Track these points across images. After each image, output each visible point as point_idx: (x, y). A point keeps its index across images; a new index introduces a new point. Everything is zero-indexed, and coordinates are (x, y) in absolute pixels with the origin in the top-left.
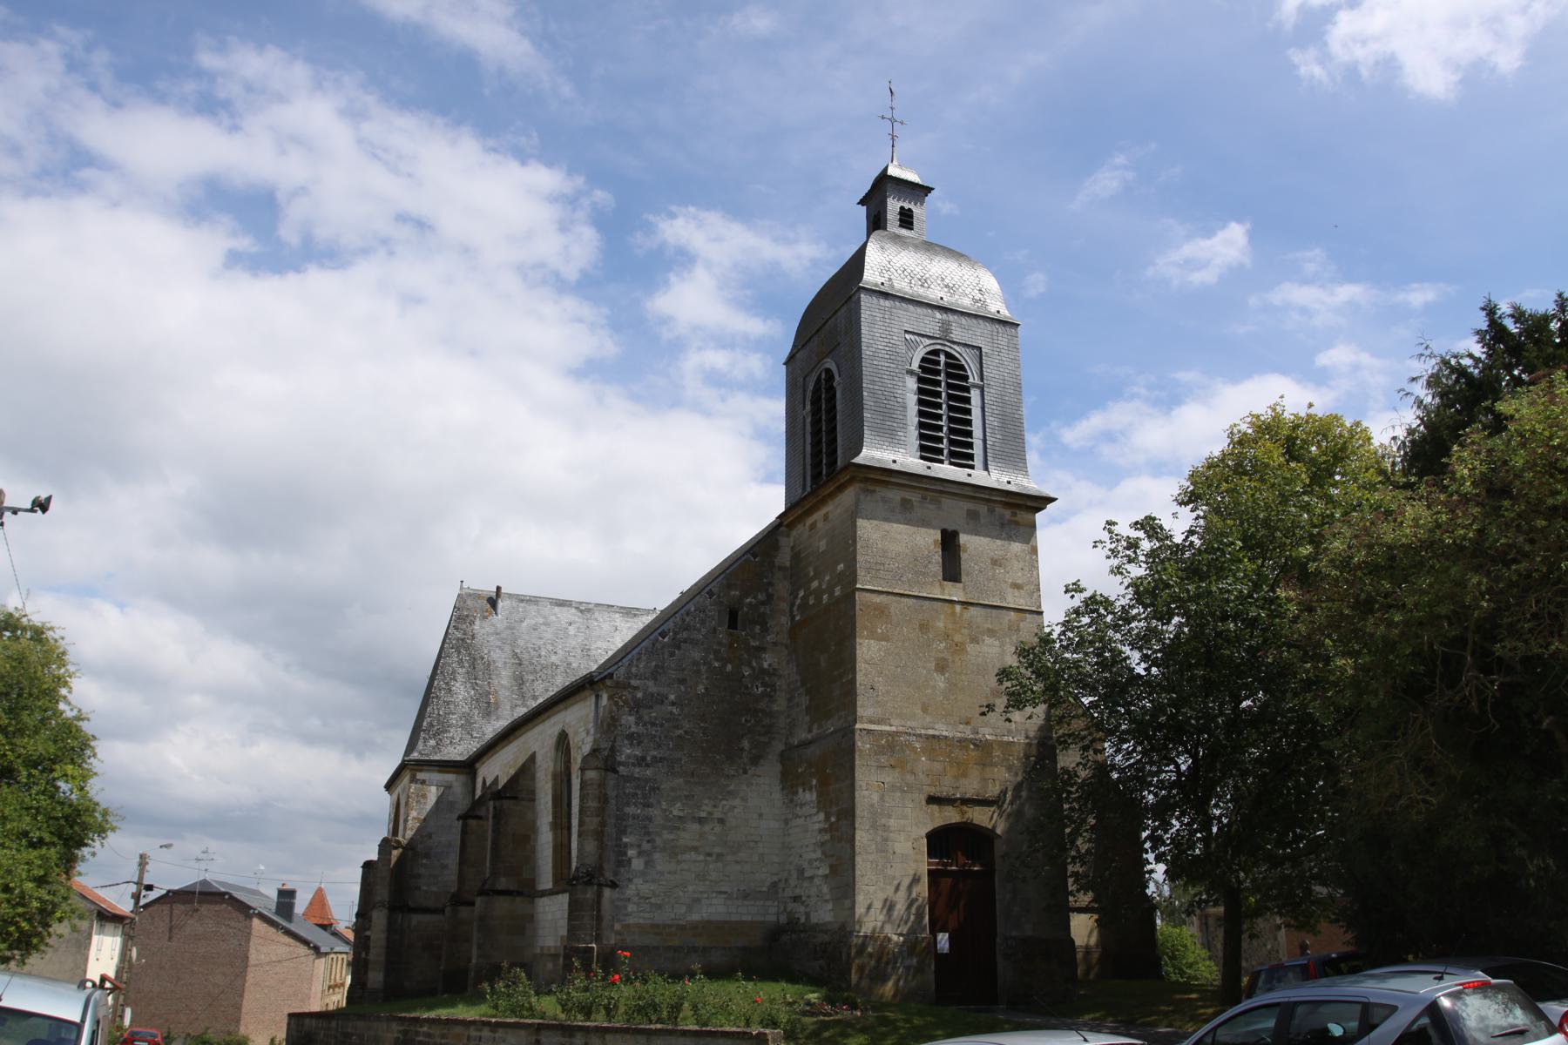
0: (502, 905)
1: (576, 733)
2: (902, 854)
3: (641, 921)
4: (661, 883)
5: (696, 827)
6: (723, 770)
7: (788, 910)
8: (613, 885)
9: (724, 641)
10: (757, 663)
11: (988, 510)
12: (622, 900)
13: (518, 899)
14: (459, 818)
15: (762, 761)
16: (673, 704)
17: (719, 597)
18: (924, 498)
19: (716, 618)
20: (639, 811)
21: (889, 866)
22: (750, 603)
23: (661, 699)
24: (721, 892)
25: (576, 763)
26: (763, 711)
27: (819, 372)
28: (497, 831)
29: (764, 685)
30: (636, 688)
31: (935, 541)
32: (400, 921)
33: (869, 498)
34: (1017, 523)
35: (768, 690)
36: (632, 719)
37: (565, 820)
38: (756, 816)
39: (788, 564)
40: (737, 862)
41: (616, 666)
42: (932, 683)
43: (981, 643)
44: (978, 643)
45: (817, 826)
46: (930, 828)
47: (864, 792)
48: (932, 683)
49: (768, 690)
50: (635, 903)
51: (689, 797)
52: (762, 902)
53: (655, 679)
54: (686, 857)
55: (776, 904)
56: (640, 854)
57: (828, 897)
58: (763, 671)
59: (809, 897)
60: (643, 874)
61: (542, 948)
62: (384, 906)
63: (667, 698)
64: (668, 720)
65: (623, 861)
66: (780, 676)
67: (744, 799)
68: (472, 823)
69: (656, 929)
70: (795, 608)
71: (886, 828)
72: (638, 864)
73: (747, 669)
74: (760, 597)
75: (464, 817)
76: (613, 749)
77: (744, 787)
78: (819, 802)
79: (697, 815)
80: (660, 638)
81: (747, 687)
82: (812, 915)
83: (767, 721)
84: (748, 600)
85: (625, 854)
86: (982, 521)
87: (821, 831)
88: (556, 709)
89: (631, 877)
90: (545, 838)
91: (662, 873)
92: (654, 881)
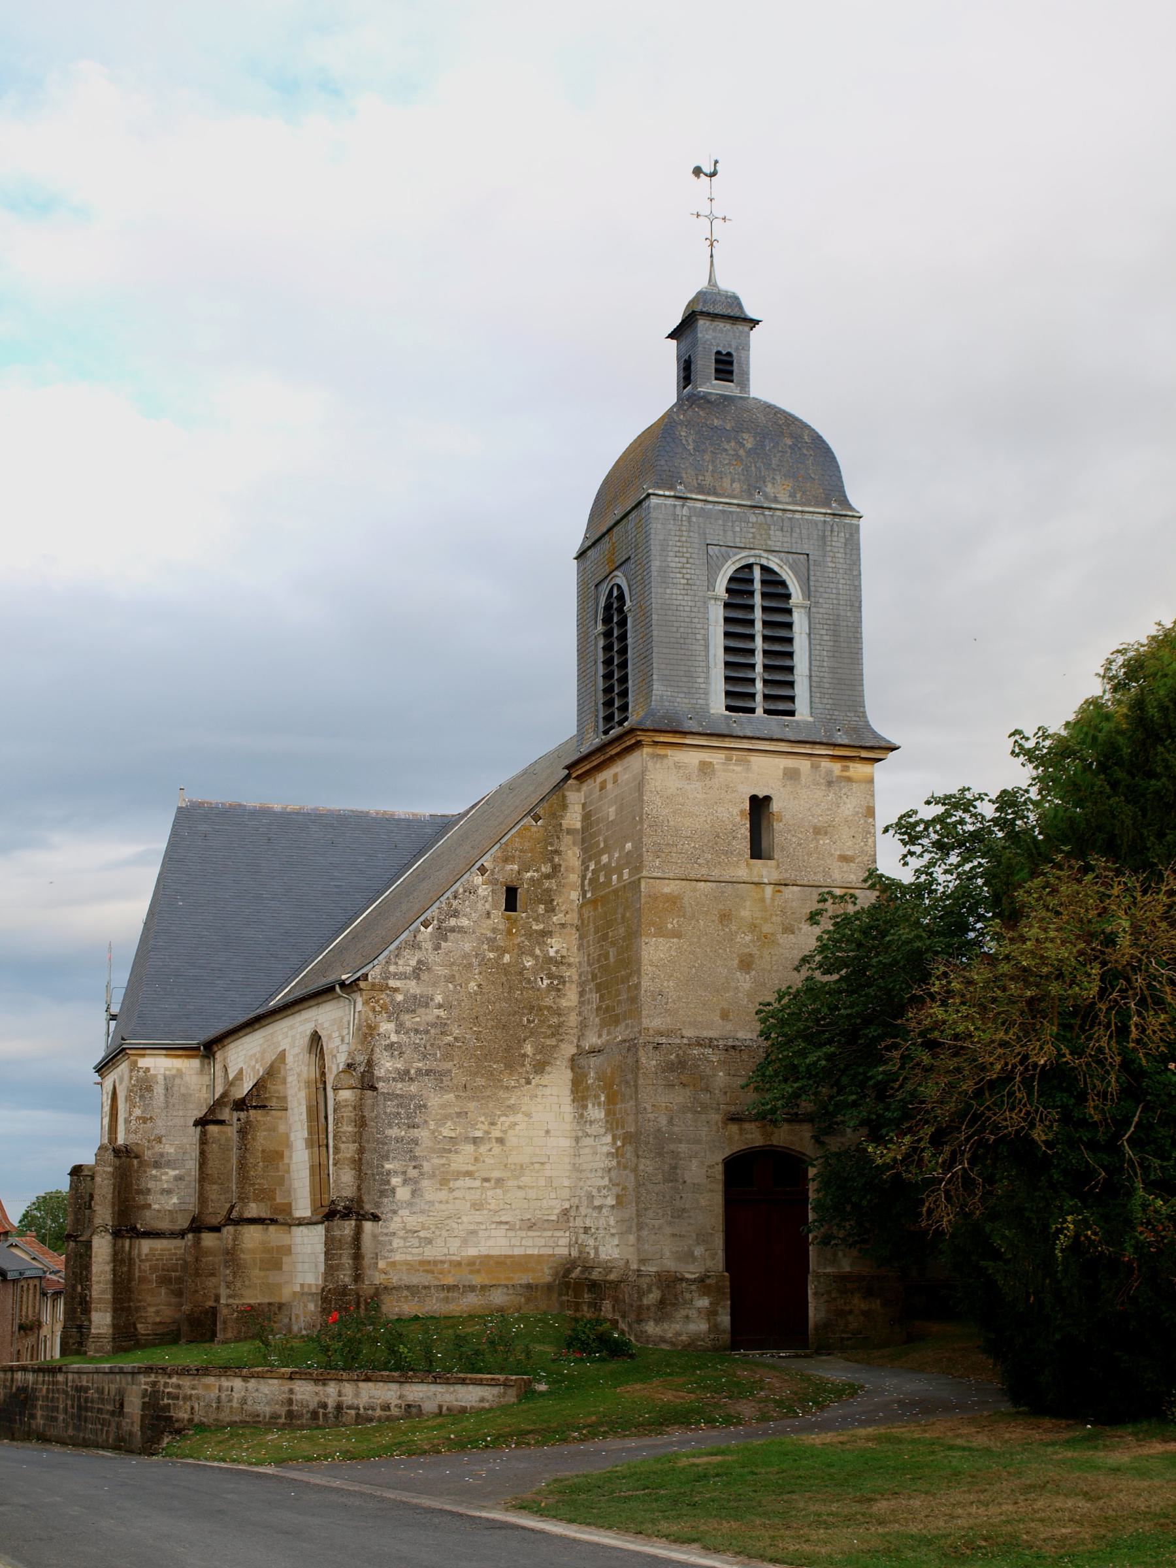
0: (252, 1236)
1: (330, 1037)
2: (694, 1184)
3: (409, 1258)
4: (432, 1214)
5: (470, 1148)
6: (500, 1081)
7: (580, 1242)
8: (375, 1218)
9: (501, 927)
10: (540, 950)
11: (812, 766)
12: (386, 1234)
13: (272, 1228)
14: (196, 1124)
15: (548, 1069)
16: (440, 1006)
17: (493, 873)
18: (729, 759)
19: (490, 898)
20: (403, 1133)
21: (678, 1197)
22: (532, 879)
23: (423, 1002)
24: (501, 1223)
25: (331, 1073)
26: (549, 1008)
27: (609, 587)
28: (244, 1146)
29: (550, 976)
30: (396, 990)
31: (742, 812)
32: (127, 1248)
33: (658, 765)
34: (849, 780)
35: (555, 982)
36: (391, 1026)
37: (322, 1136)
38: (542, 1133)
39: (578, 825)
40: (519, 1187)
41: (371, 965)
42: (733, 984)
43: (797, 932)
44: (793, 933)
45: (605, 1149)
46: (727, 1153)
47: (649, 1115)
48: (733, 984)
49: (555, 982)
50: (401, 1238)
51: (462, 1114)
52: (549, 1234)
53: (418, 978)
54: (459, 1183)
55: (567, 1234)
56: (405, 1182)
57: (613, 1231)
58: (550, 960)
59: (597, 1229)
60: (410, 1204)
61: (302, 1285)
62: (107, 1231)
63: (432, 1000)
64: (434, 1025)
65: (386, 1190)
66: (569, 965)
67: (528, 1115)
68: (213, 1129)
69: (427, 1266)
70: (586, 882)
71: (675, 1155)
72: (403, 1193)
73: (529, 958)
74: (543, 869)
75: (201, 1123)
76: (370, 1064)
77: (526, 1099)
78: (607, 1121)
79: (471, 1135)
80: (422, 928)
81: (529, 981)
82: (601, 1248)
83: (554, 1020)
84: (529, 874)
85: (388, 1182)
86: (803, 781)
87: (609, 1154)
88: (306, 1004)
89: (396, 1208)
90: (300, 1159)
91: (432, 1203)
92: (422, 1212)
